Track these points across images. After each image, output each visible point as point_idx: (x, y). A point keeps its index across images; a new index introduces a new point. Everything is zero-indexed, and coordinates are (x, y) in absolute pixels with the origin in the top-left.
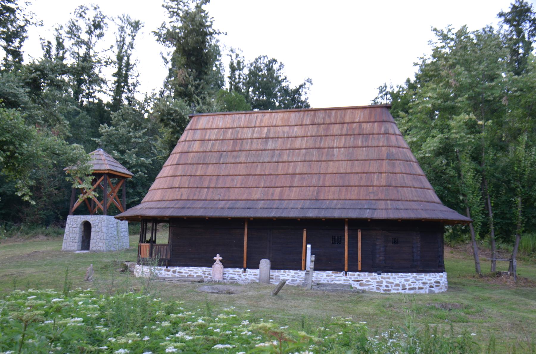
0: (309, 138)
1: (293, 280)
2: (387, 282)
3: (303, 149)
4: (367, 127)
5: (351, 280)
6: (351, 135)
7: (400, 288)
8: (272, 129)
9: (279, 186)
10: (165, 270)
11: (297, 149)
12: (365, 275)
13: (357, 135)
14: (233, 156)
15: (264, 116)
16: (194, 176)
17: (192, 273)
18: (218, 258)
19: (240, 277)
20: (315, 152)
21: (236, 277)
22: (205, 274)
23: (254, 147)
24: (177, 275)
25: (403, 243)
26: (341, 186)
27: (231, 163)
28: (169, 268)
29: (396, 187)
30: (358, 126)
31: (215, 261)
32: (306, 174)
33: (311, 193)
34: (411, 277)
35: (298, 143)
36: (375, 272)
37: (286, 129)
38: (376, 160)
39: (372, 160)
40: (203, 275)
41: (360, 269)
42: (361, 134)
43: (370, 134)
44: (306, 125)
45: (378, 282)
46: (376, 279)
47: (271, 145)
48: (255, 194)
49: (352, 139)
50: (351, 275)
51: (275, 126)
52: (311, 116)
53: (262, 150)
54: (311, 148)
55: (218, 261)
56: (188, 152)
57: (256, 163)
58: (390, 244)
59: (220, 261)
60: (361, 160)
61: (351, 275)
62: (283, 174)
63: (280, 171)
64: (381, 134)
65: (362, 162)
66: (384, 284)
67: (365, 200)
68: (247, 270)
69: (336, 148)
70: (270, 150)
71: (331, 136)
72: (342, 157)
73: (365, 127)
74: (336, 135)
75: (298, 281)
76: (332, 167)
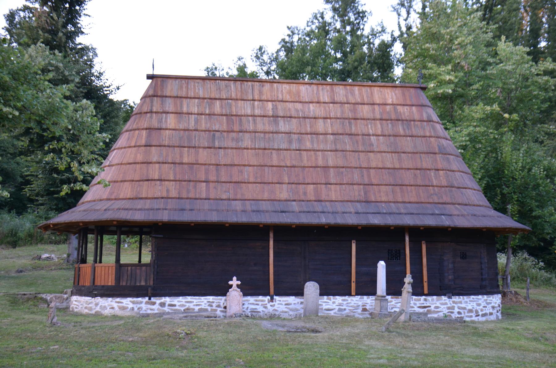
0: (333, 120)
1: (340, 310)
2: (459, 308)
3: (329, 134)
4: (405, 111)
5: (415, 307)
6: (388, 120)
7: (473, 314)
8: (280, 106)
9: (310, 182)
10: (147, 303)
11: (321, 134)
12: (433, 300)
13: (394, 120)
14: (233, 139)
15: (263, 86)
16: (179, 164)
17: (191, 306)
18: (235, 282)
19: (266, 308)
20: (347, 139)
21: (260, 308)
22: (212, 306)
23: (260, 127)
24: (166, 309)
25: (449, 257)
26: (393, 185)
27: (232, 148)
28: (153, 299)
29: (459, 188)
30: (392, 110)
31: (231, 286)
32: (343, 167)
33: (357, 192)
34: (483, 300)
35: (320, 126)
36: (445, 295)
37: (299, 106)
38: (427, 153)
39: (422, 153)
40: (209, 308)
41: (426, 291)
42: (399, 120)
43: (411, 121)
44: (324, 103)
45: (449, 308)
46: (446, 304)
47: (283, 126)
48: (280, 193)
49: (390, 125)
50: (415, 300)
51: (282, 101)
52: (327, 91)
53: (272, 133)
54: (341, 134)
55: (234, 286)
56: (160, 129)
57: (270, 149)
58: (459, 259)
59: (238, 286)
60: (409, 153)
61: (415, 300)
62: (311, 167)
63: (305, 163)
64: (424, 121)
65: (410, 155)
66: (456, 310)
67: (429, 203)
68: (275, 297)
69: (373, 135)
70: (284, 133)
71: (362, 119)
72: (384, 148)
73: (402, 111)
74: (369, 119)
75: (347, 311)
76: (375, 160)
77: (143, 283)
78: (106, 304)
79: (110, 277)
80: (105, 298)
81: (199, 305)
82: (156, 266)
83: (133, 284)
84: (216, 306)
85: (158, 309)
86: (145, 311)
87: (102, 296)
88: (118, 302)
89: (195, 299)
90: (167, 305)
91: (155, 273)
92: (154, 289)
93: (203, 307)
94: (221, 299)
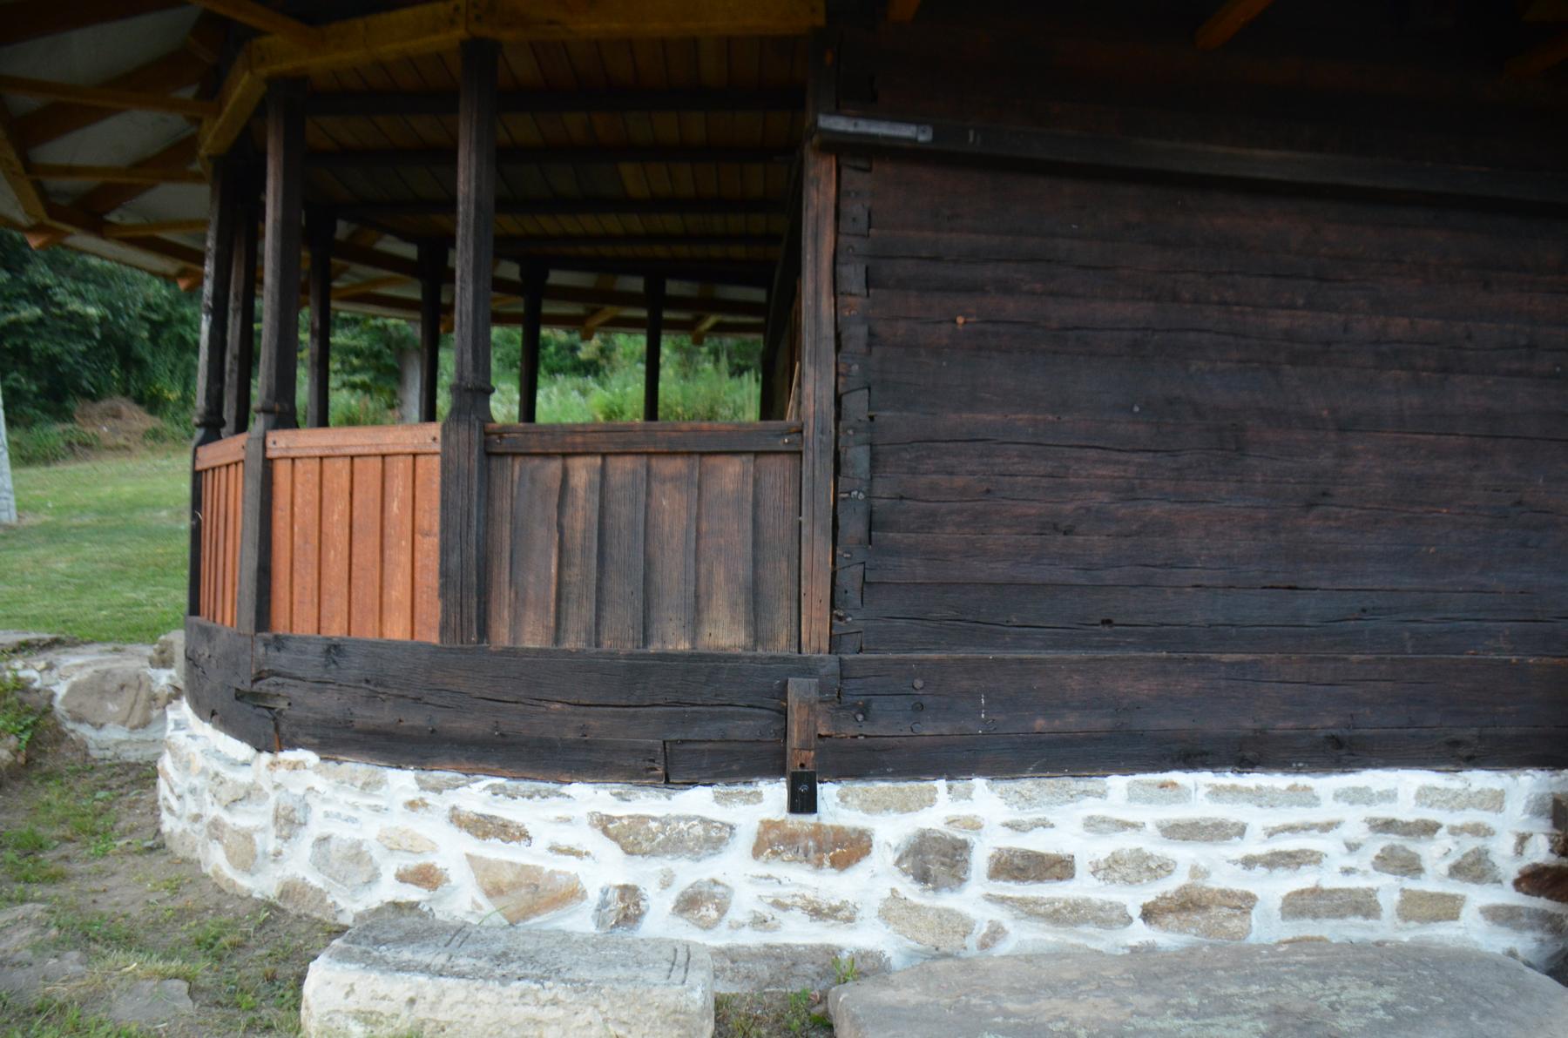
10: (770, 842)
22: (1411, 866)
28: (838, 804)
40: (1388, 888)
77: (725, 633)
78: (369, 831)
79: (399, 557)
80: (356, 768)
81: (1292, 860)
82: (858, 456)
83: (619, 638)
84: (1457, 871)
85: (893, 911)
86: (760, 922)
87: (337, 739)
88: (483, 827)
89: (1258, 797)
90: (980, 860)
91: (854, 527)
92: (841, 693)
93: (1329, 878)
94: (1496, 801)
